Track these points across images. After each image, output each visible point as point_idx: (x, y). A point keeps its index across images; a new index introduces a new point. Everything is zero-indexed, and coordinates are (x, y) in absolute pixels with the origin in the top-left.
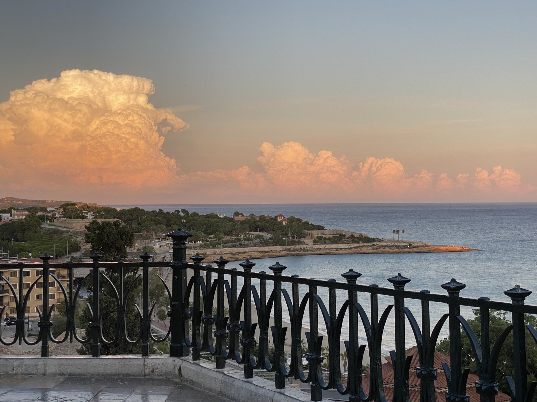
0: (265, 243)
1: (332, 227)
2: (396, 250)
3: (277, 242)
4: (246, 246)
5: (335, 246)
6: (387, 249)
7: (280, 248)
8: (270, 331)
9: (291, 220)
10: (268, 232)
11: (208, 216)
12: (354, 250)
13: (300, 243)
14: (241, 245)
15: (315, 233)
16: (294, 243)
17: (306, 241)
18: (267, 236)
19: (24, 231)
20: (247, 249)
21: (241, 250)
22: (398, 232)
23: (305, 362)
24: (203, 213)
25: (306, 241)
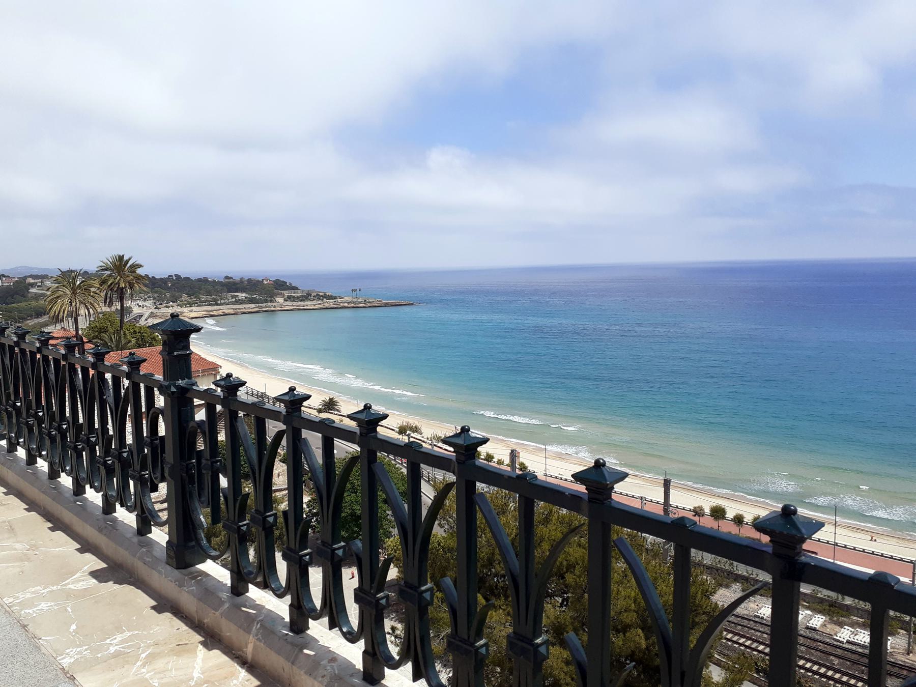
0: (241, 302)
1: (304, 287)
2: (353, 305)
3: (251, 301)
4: (221, 304)
5: (302, 303)
6: (346, 305)
7: (253, 306)
8: (695, 486)
9: (249, 280)
10: (242, 292)
11: (199, 280)
12: (317, 306)
13: (271, 301)
14: (217, 304)
15: (286, 293)
16: (266, 301)
17: (277, 299)
18: (242, 295)
19: (12, 296)
20: (221, 307)
21: (216, 308)
22: (356, 291)
23: (160, 401)
24: (193, 277)
25: (277, 299)
